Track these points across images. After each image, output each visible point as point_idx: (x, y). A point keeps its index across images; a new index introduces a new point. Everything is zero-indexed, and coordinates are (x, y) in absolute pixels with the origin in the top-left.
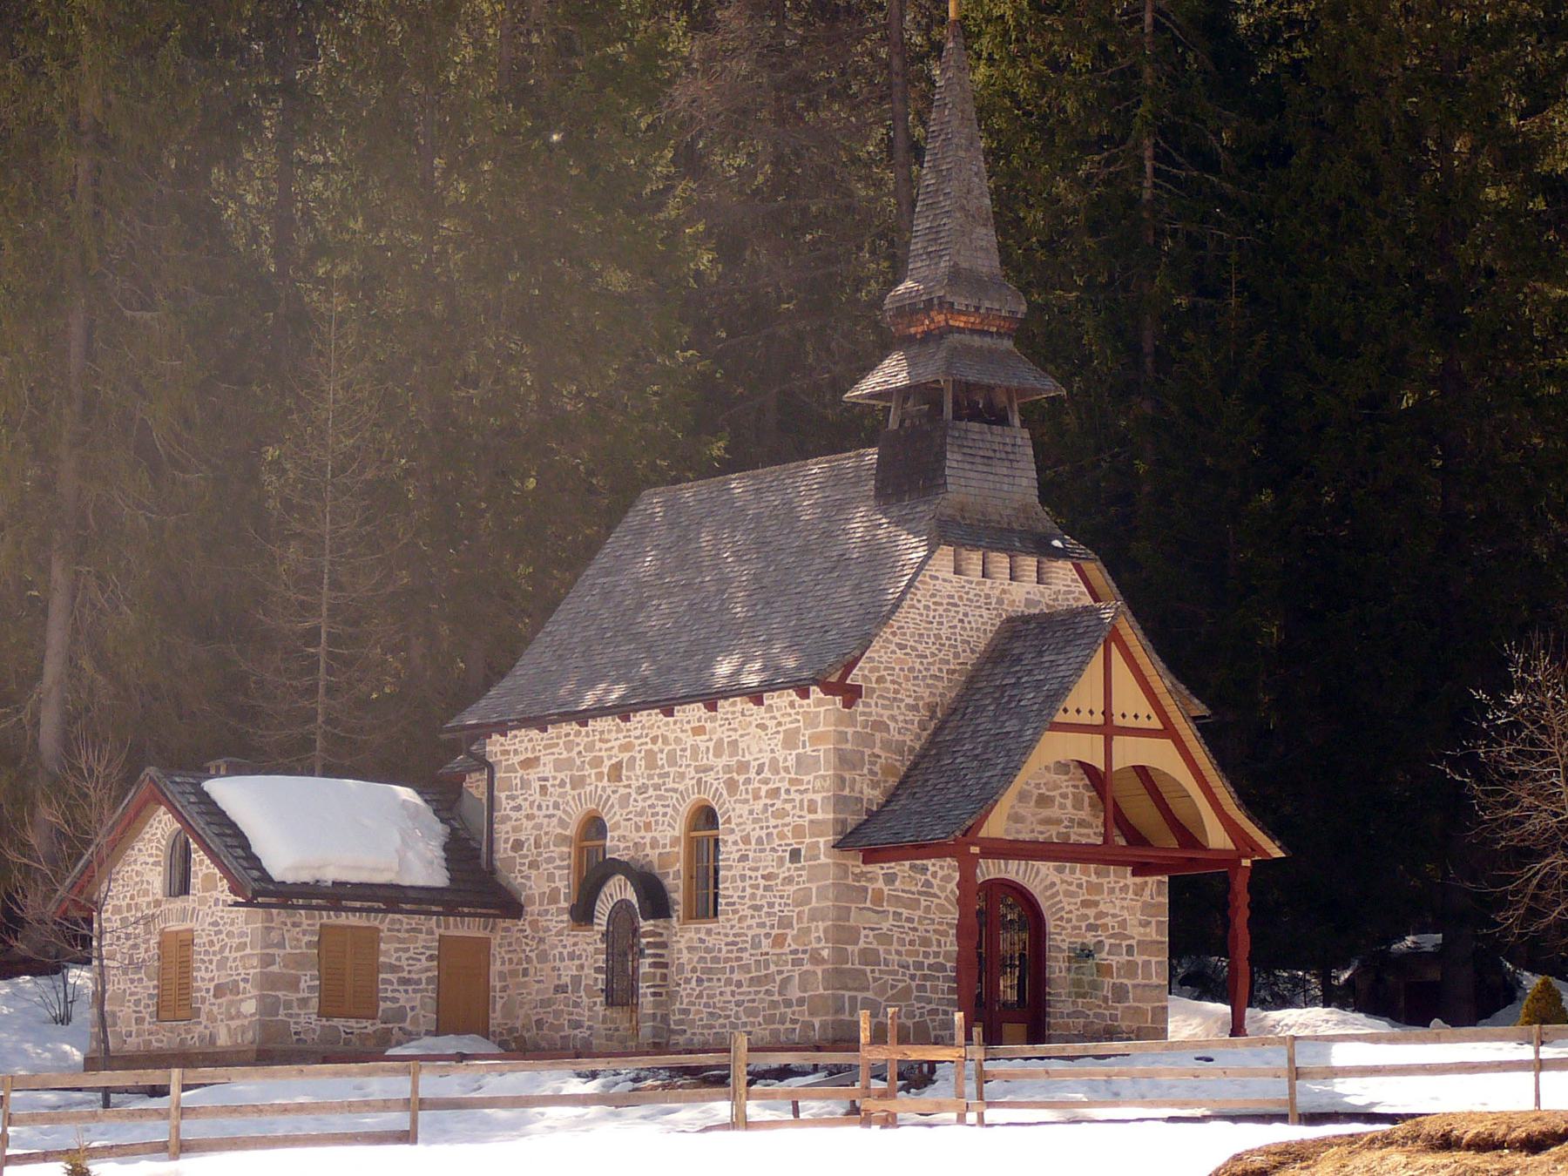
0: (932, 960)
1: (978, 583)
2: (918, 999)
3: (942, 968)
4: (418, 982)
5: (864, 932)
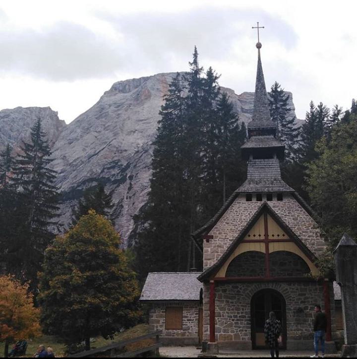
0: (240, 315)
3: (245, 317)
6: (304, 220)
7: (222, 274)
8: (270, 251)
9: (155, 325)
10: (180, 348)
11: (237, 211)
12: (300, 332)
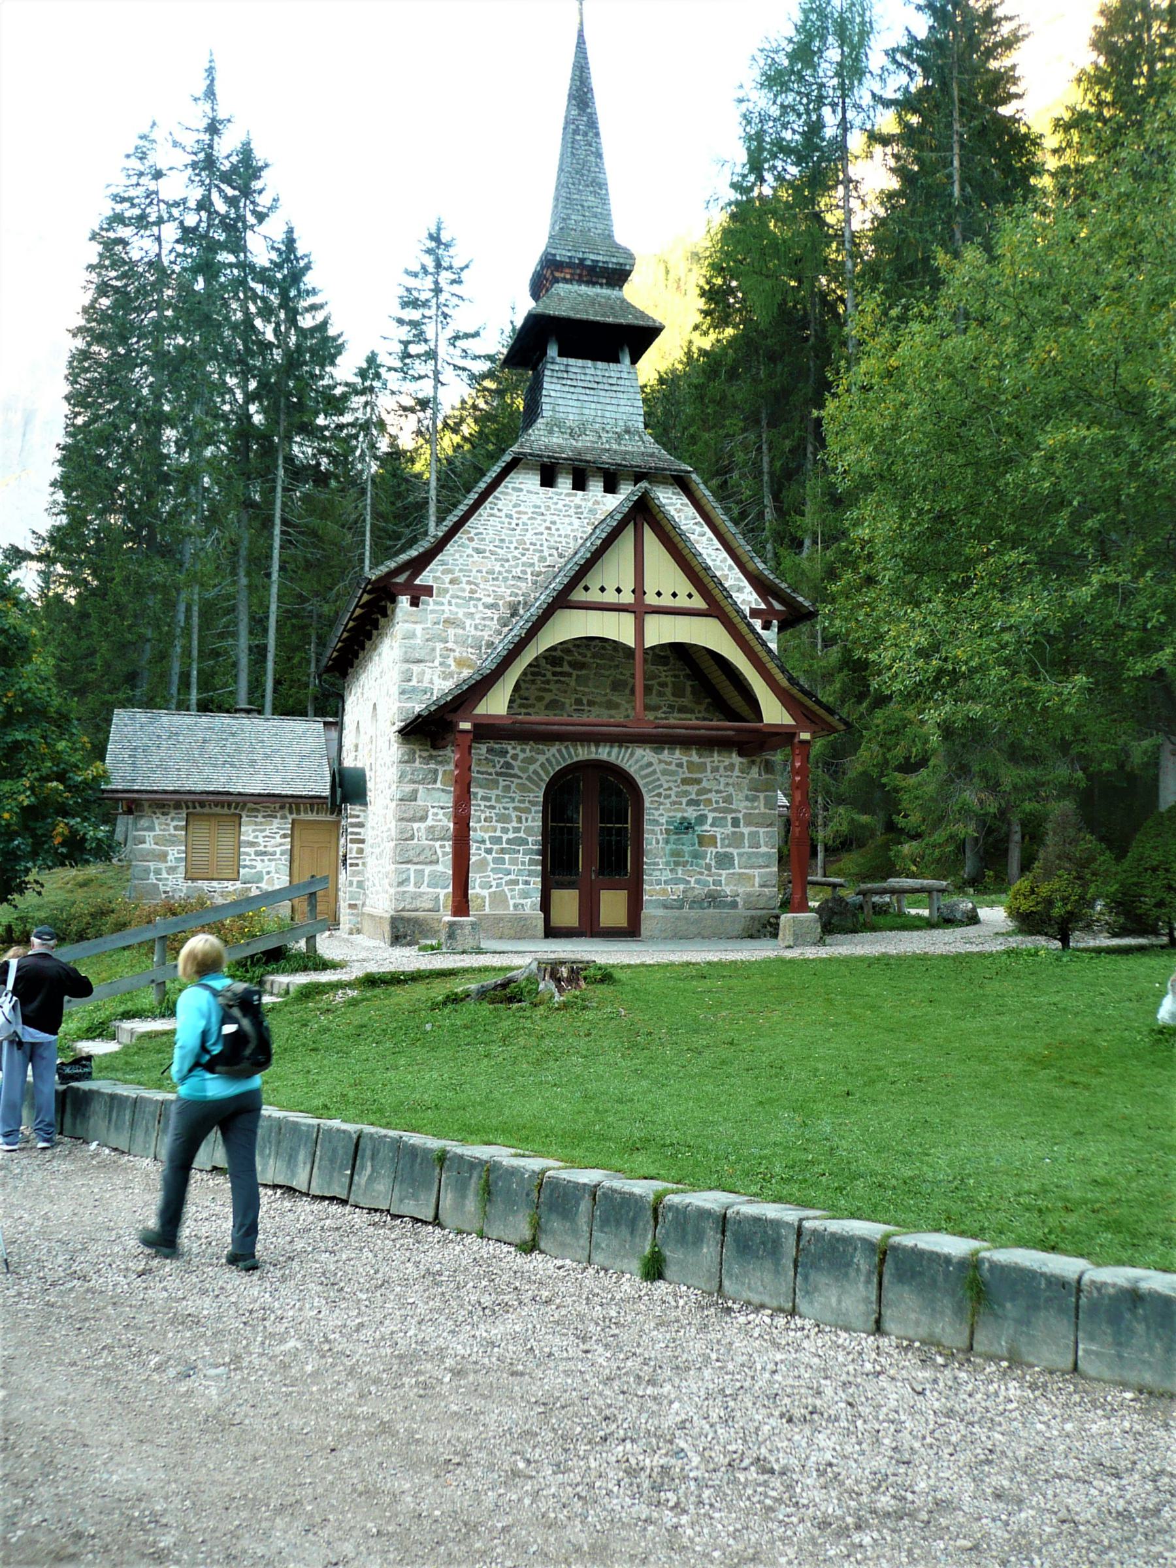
0: (511, 835)
1: (568, 495)
3: (524, 842)
4: (274, 854)
5: (432, 811)
7: (496, 704)
8: (651, 641)
9: (152, 865)
10: (850, 936)
11: (509, 516)
12: (682, 887)
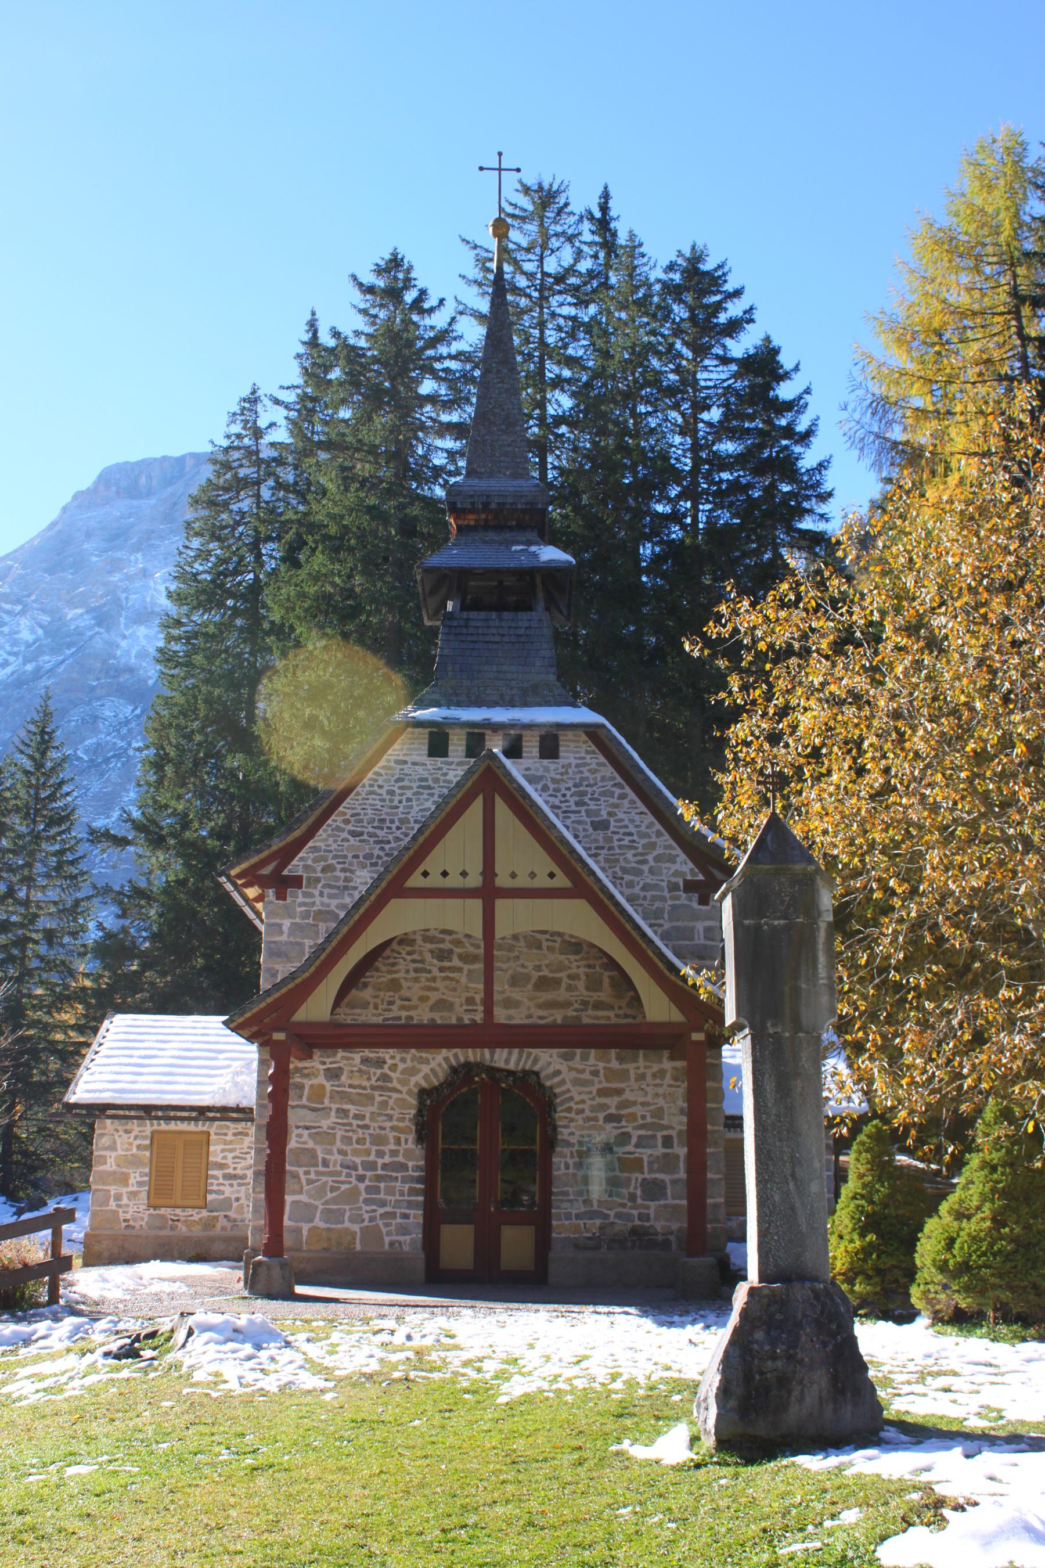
0: (387, 1159)
2: (367, 1201)
3: (403, 1167)
6: (632, 829)
7: (317, 1007)
9: (113, 1190)
12: (598, 1222)
